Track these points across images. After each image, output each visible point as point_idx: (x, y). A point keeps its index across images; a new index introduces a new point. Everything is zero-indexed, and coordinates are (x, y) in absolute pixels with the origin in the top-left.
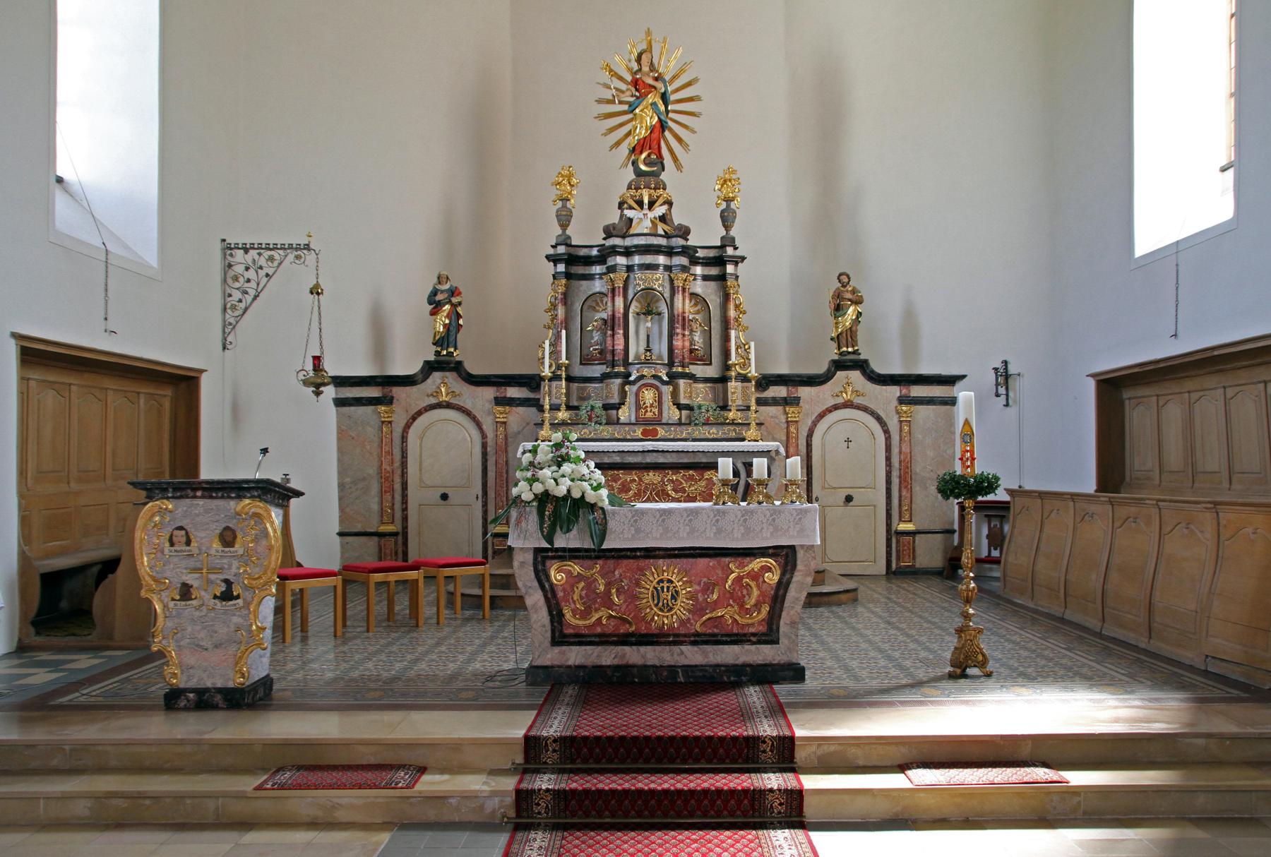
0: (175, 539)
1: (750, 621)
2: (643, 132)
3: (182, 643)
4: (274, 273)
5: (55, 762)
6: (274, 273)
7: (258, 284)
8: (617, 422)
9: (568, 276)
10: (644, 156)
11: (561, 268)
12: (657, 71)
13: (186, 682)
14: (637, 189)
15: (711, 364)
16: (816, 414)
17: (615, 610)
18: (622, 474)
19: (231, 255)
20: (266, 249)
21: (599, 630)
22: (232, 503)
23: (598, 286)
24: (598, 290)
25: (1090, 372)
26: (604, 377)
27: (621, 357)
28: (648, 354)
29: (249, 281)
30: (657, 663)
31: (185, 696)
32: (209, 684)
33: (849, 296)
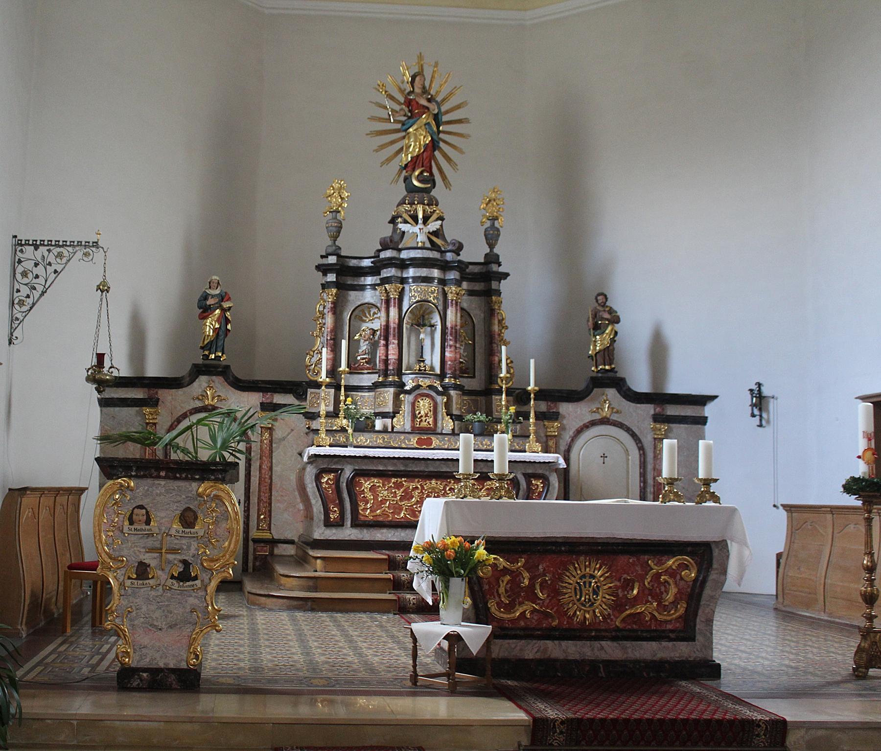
0: (134, 517)
1: (669, 618)
2: (417, 150)
3: (136, 622)
4: (62, 270)
6: (62, 270)
7: (46, 281)
9: (337, 285)
10: (417, 173)
11: (331, 277)
12: (429, 94)
13: (138, 662)
15: (474, 377)
16: (574, 429)
17: (538, 604)
18: (405, 481)
19: (21, 251)
20: (56, 245)
21: (522, 623)
22: (194, 485)
23: (369, 296)
24: (366, 301)
25: (860, 394)
26: (375, 386)
28: (422, 364)
29: (37, 277)
30: (577, 657)
31: (139, 675)
32: (162, 665)
33: (606, 316)
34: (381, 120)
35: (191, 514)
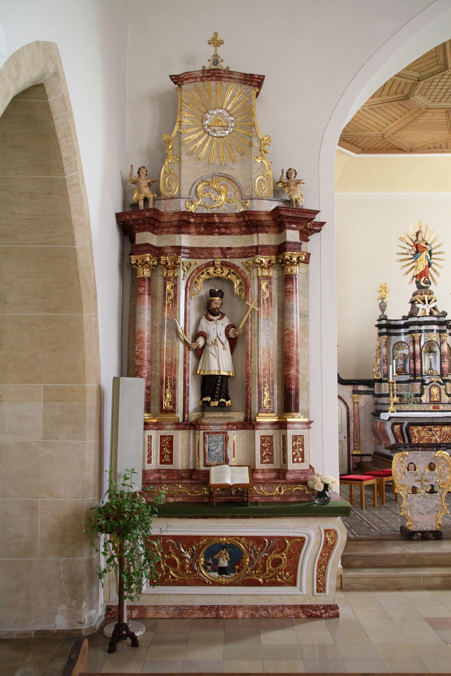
3: (413, 512)
5: (403, 563)
8: (420, 403)
10: (423, 279)
11: (384, 330)
14: (421, 294)
22: (433, 453)
23: (403, 338)
26: (409, 381)
27: (419, 372)
28: (431, 370)
32: (425, 529)
34: (403, 254)
35: (433, 465)
